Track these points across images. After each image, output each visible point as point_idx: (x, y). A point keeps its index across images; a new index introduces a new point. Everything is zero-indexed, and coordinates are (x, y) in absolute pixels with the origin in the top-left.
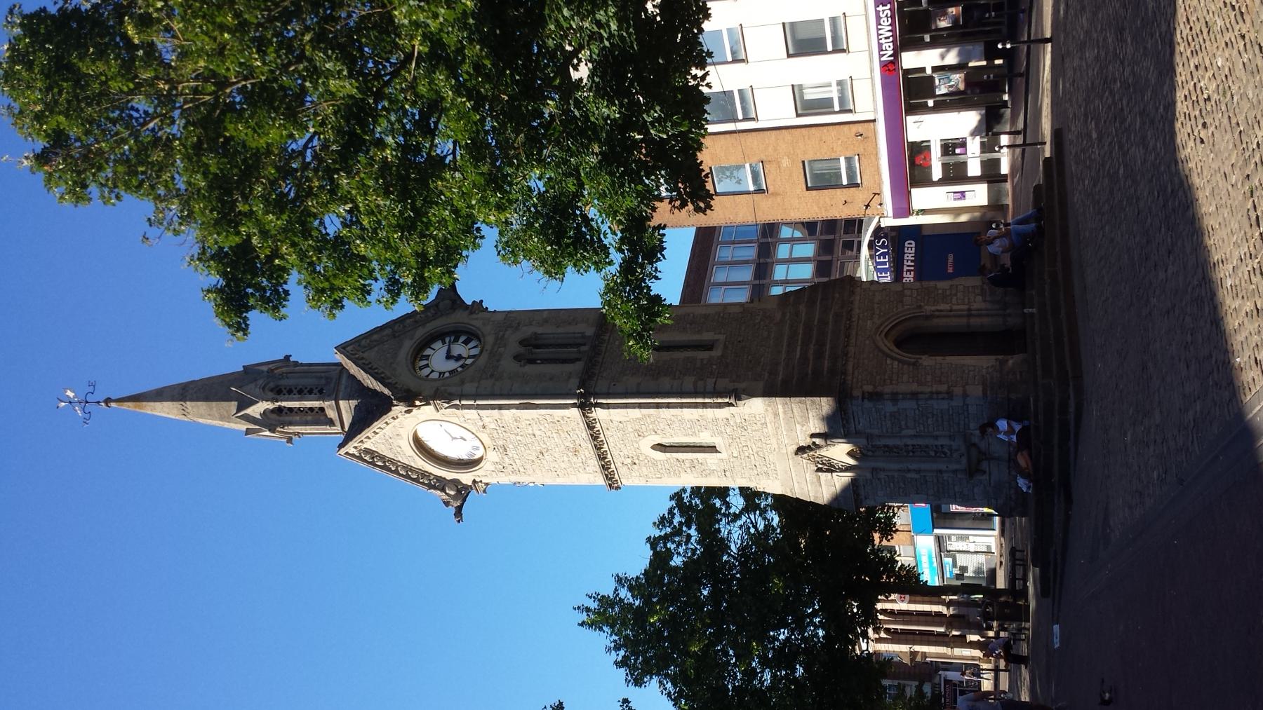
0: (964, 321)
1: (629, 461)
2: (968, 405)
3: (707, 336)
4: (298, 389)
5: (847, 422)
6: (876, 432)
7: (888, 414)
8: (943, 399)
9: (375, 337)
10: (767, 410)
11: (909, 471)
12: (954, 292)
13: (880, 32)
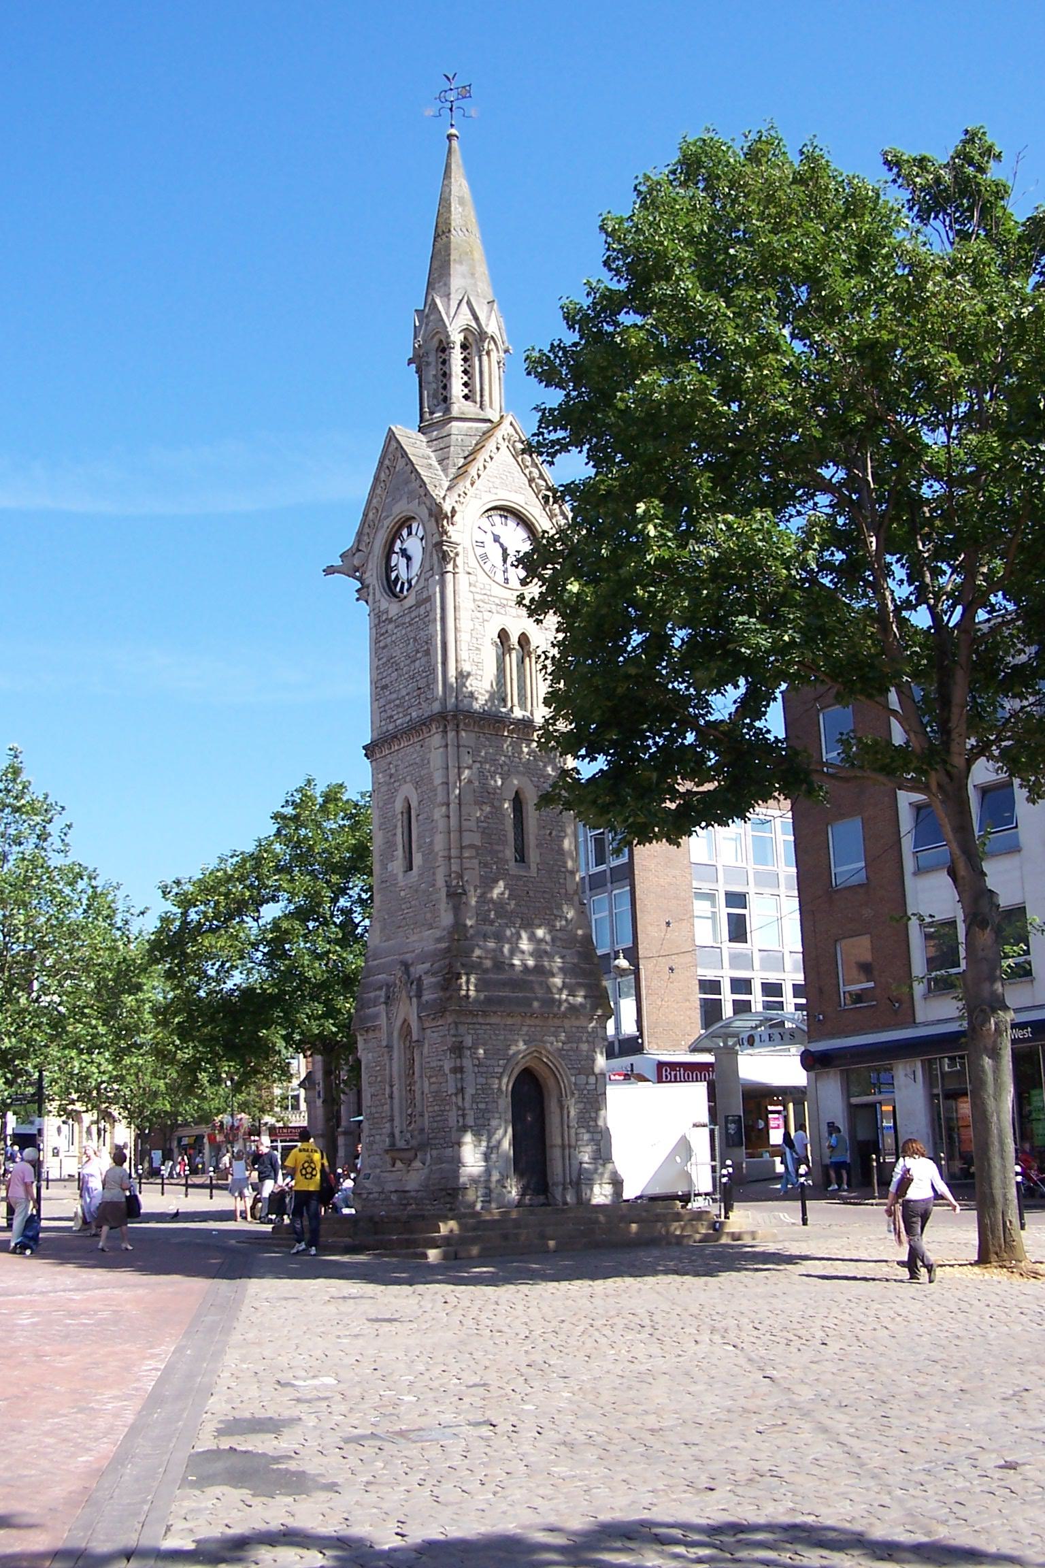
0: (558, 1141)
1: (393, 771)
3: (533, 856)
4: (468, 369)
5: (433, 1019)
6: (425, 1050)
8: (458, 1121)
11: (391, 1086)
12: (591, 1129)
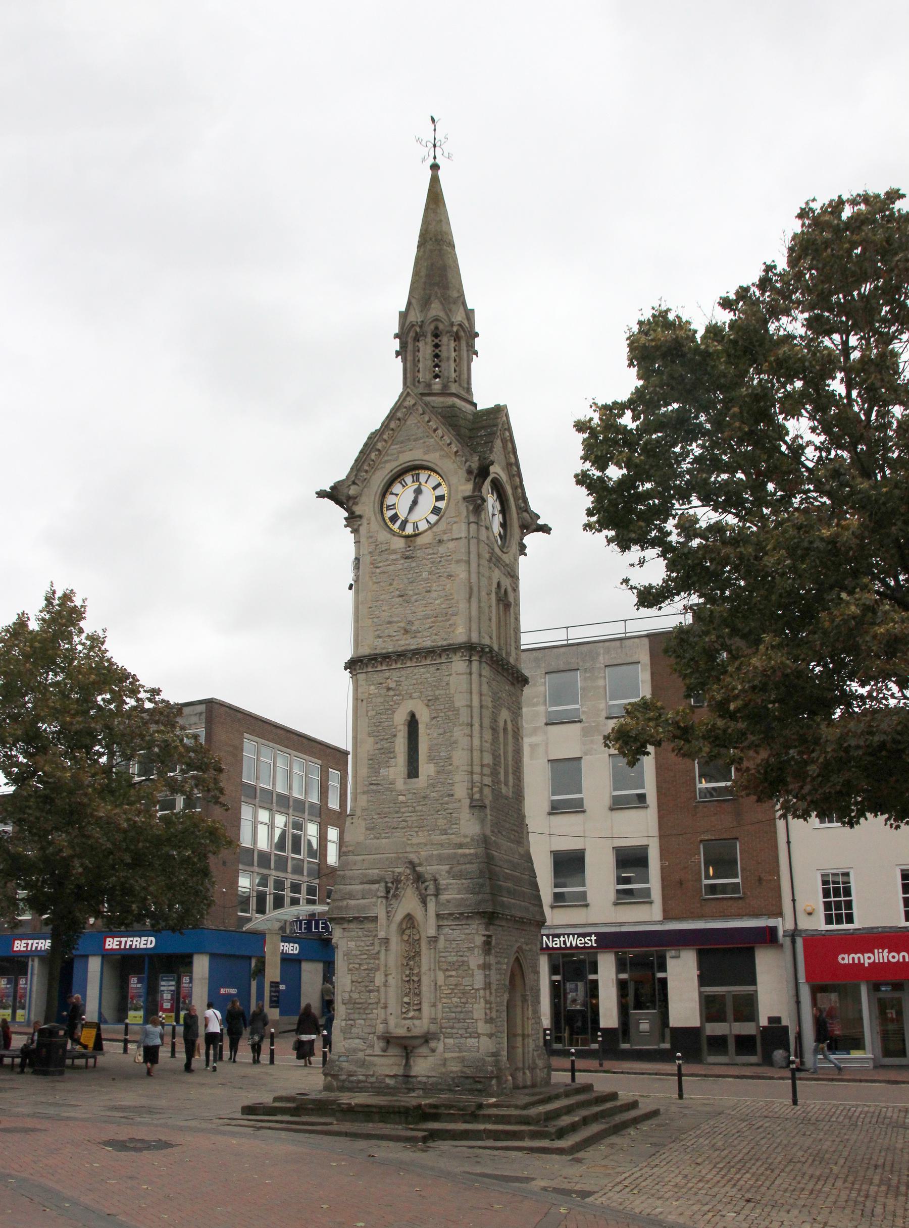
2: (478, 1037)
3: (426, 769)
7: (465, 959)
8: (486, 1014)
9: (510, 445)
10: (466, 836)
13: (571, 937)
